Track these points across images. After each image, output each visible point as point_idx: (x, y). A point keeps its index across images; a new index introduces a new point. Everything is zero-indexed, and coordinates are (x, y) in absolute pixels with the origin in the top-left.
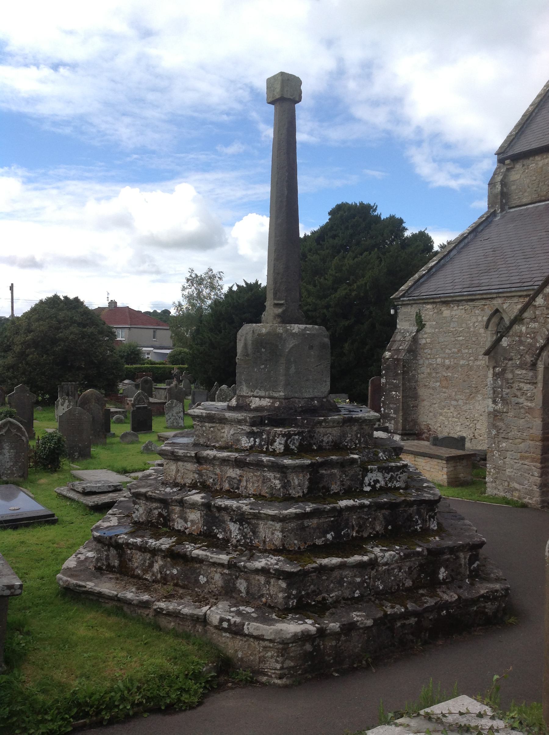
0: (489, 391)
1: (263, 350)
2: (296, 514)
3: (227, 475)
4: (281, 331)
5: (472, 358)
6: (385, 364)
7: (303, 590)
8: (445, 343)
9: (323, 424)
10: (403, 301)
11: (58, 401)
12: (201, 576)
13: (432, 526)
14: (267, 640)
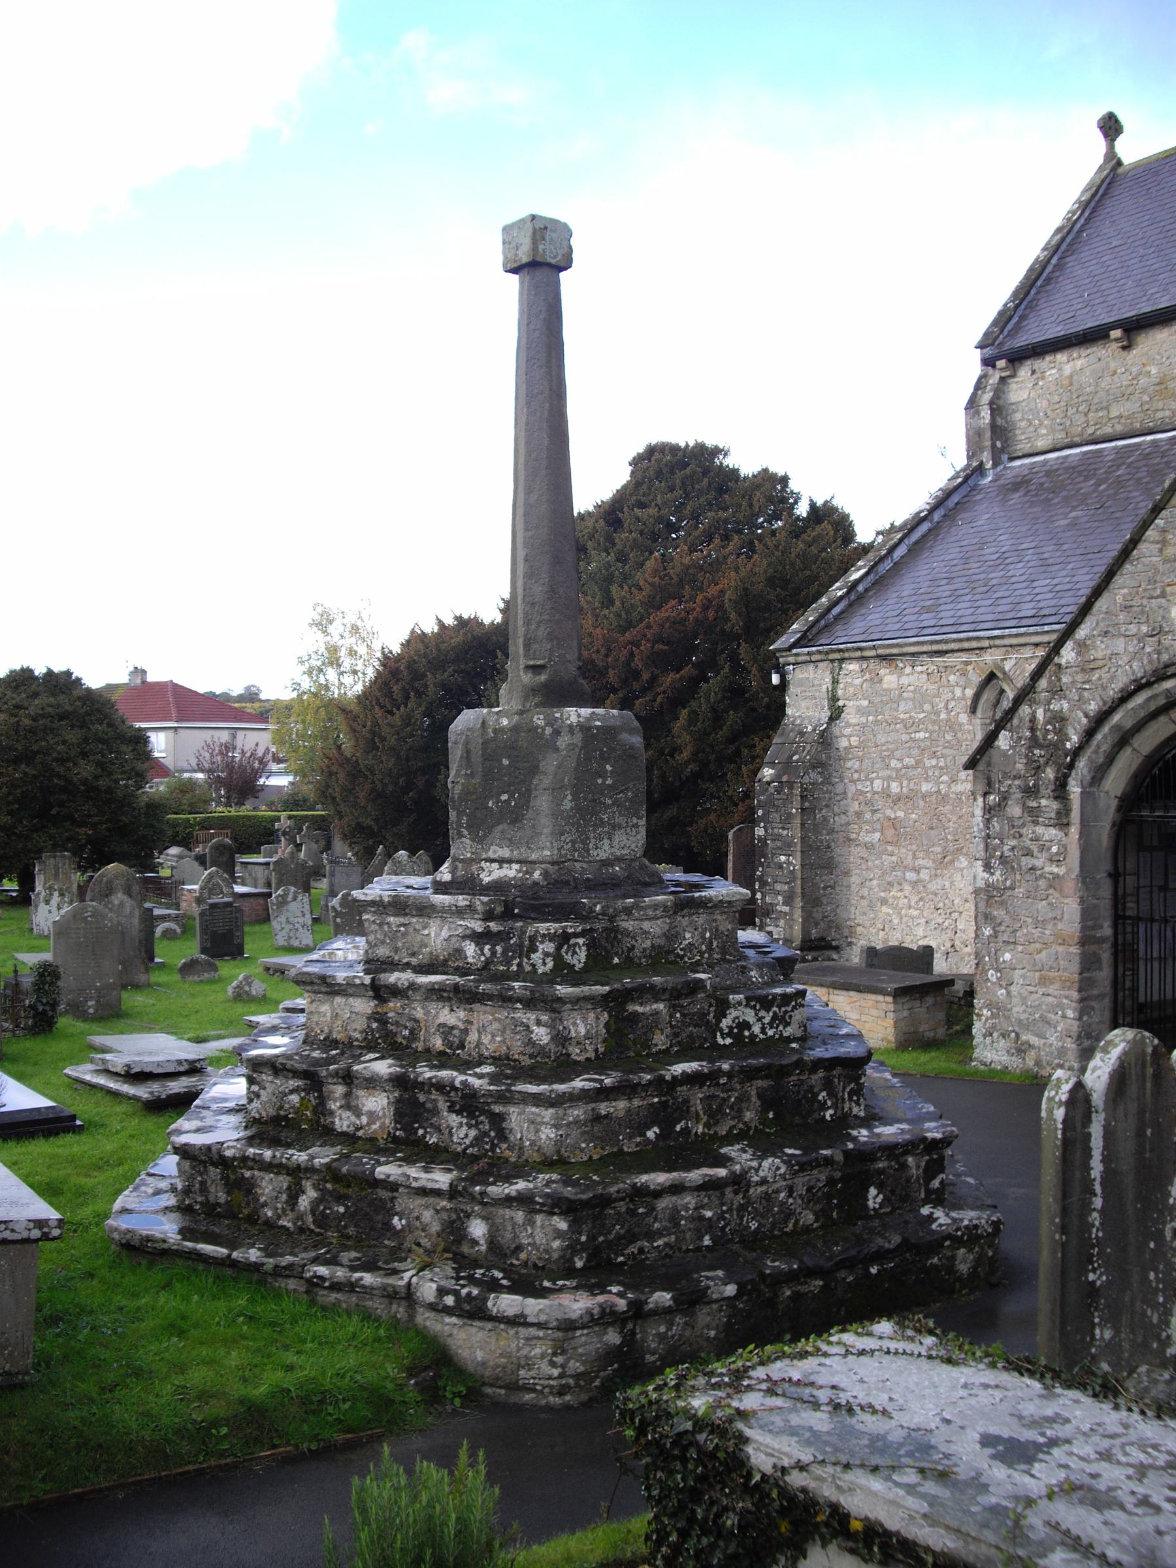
0: (978, 848)
2: (583, 1090)
3: (438, 1021)
4: (541, 722)
5: (945, 778)
6: (763, 794)
8: (891, 746)
10: (797, 655)
11: (39, 894)
12: (396, 1218)
13: (855, 1110)
14: (533, 1325)
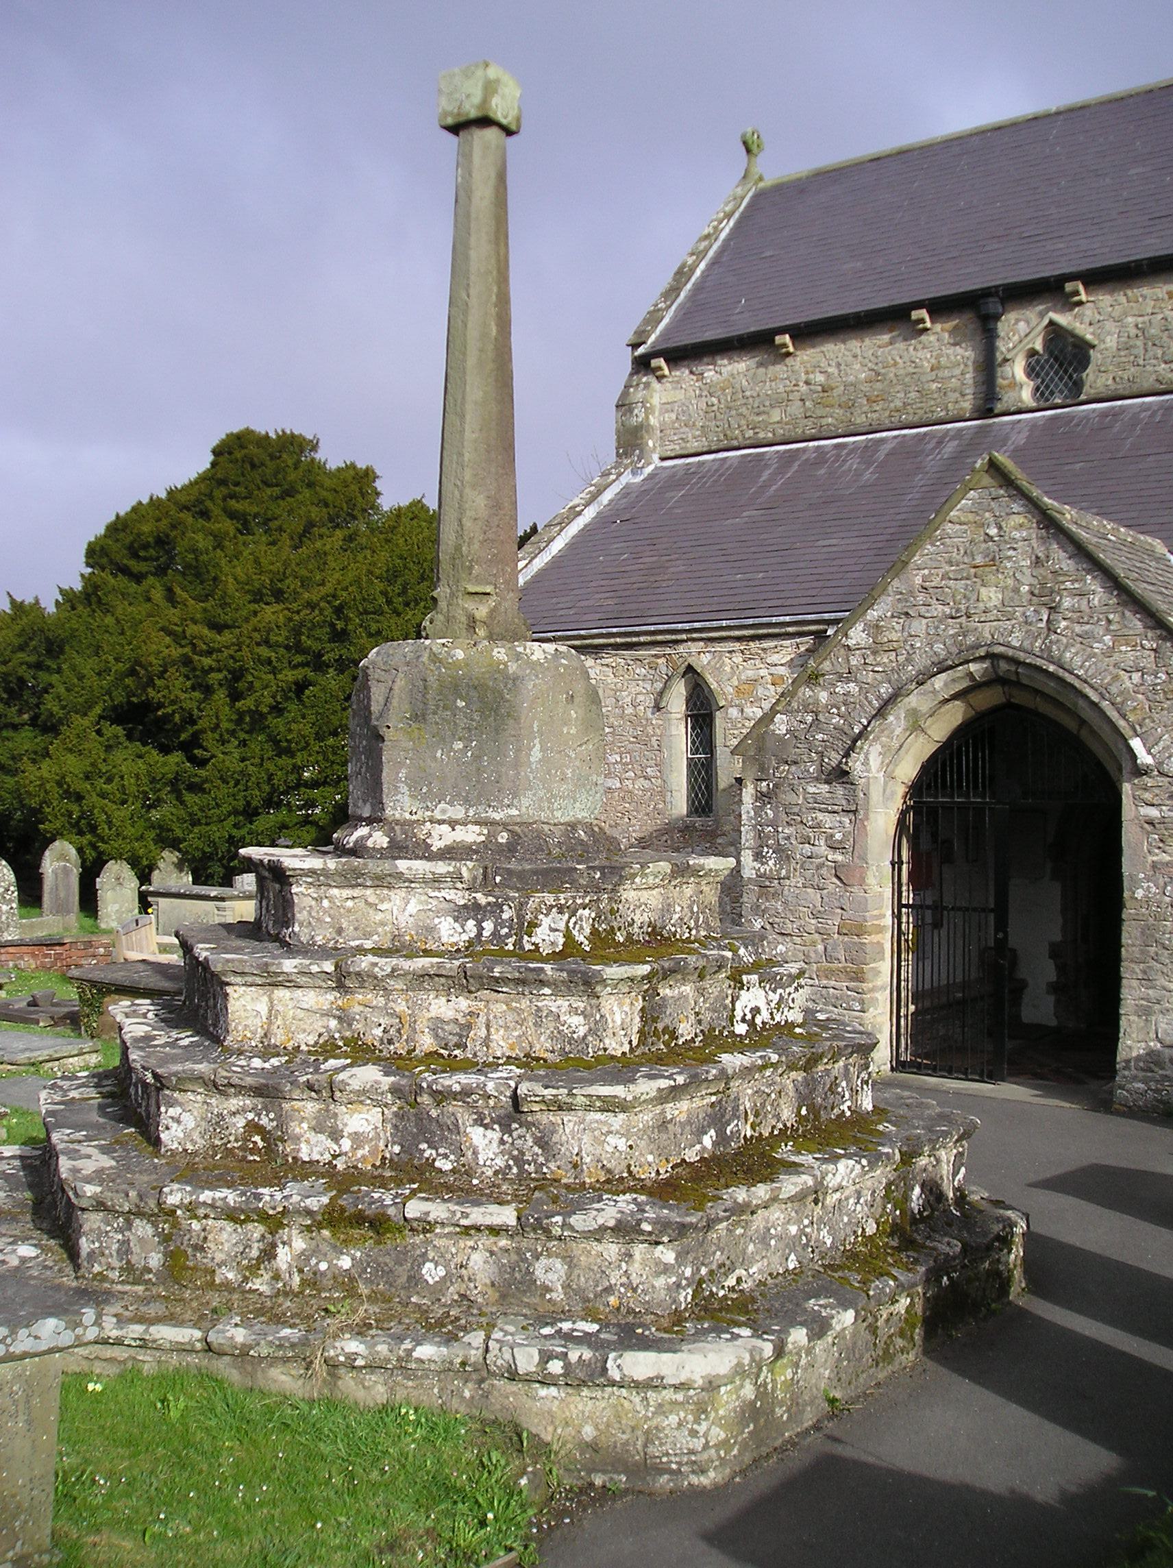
1: (461, 704)
7: (703, 1264)
9: (637, 880)
